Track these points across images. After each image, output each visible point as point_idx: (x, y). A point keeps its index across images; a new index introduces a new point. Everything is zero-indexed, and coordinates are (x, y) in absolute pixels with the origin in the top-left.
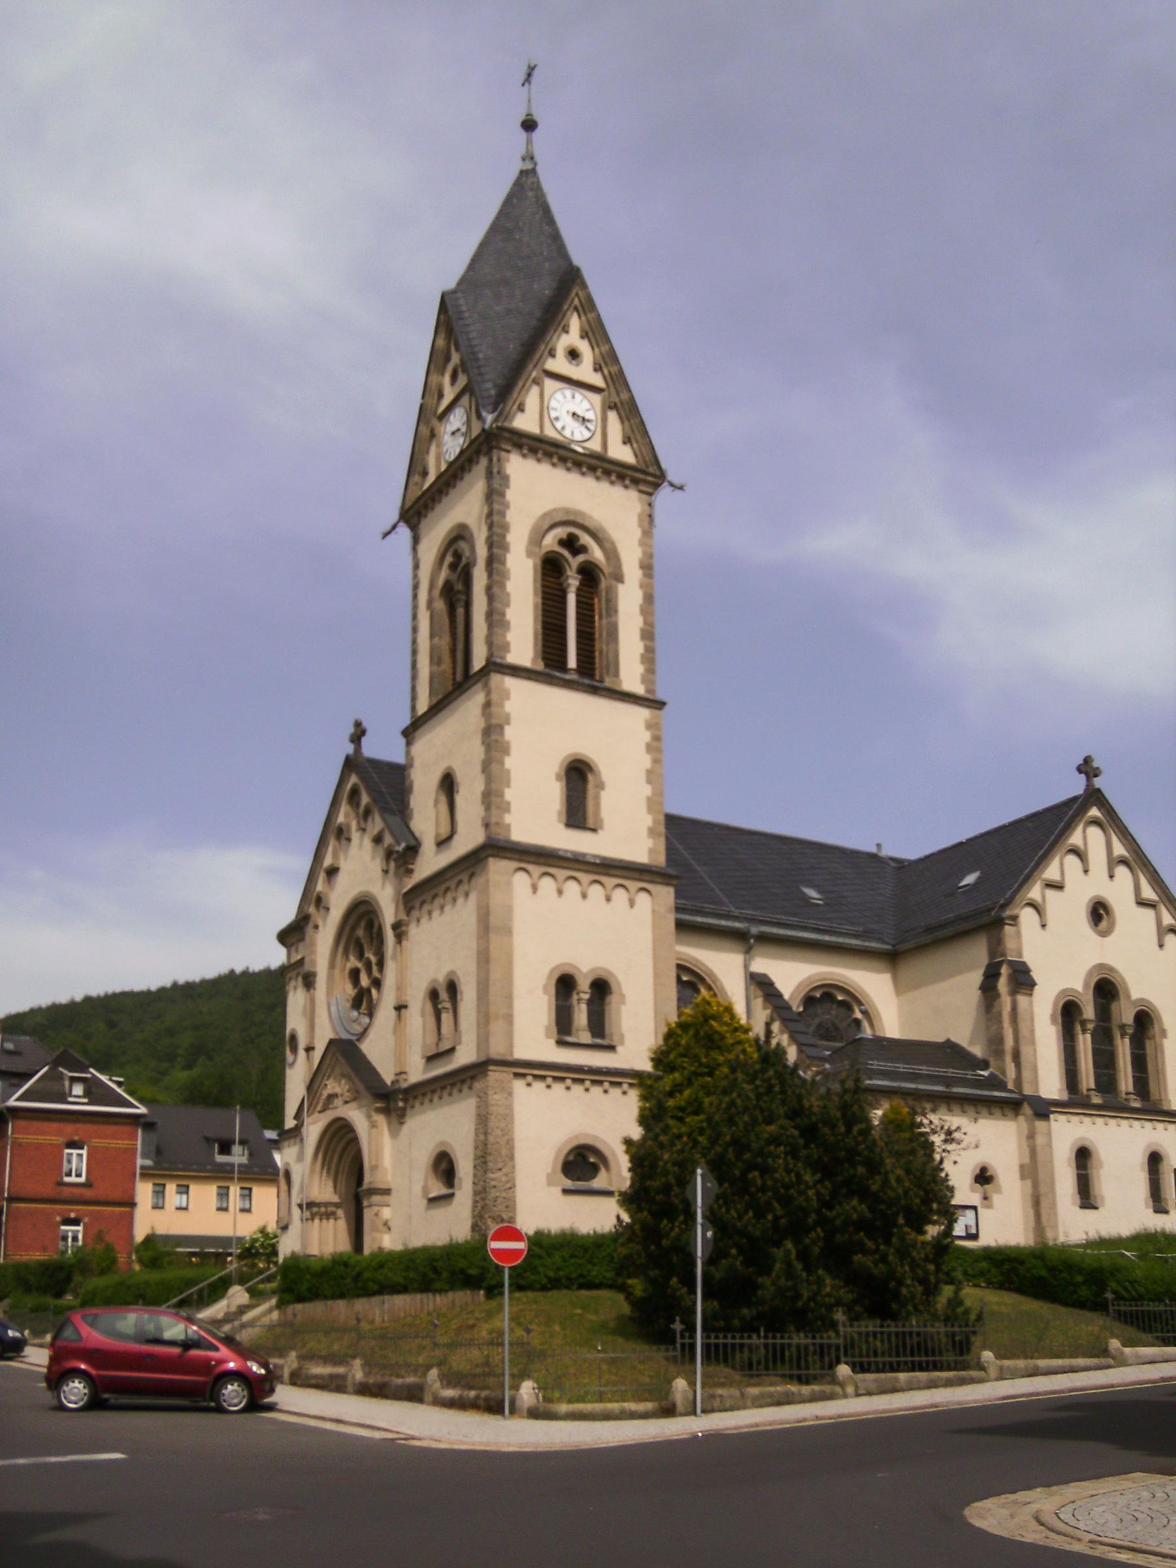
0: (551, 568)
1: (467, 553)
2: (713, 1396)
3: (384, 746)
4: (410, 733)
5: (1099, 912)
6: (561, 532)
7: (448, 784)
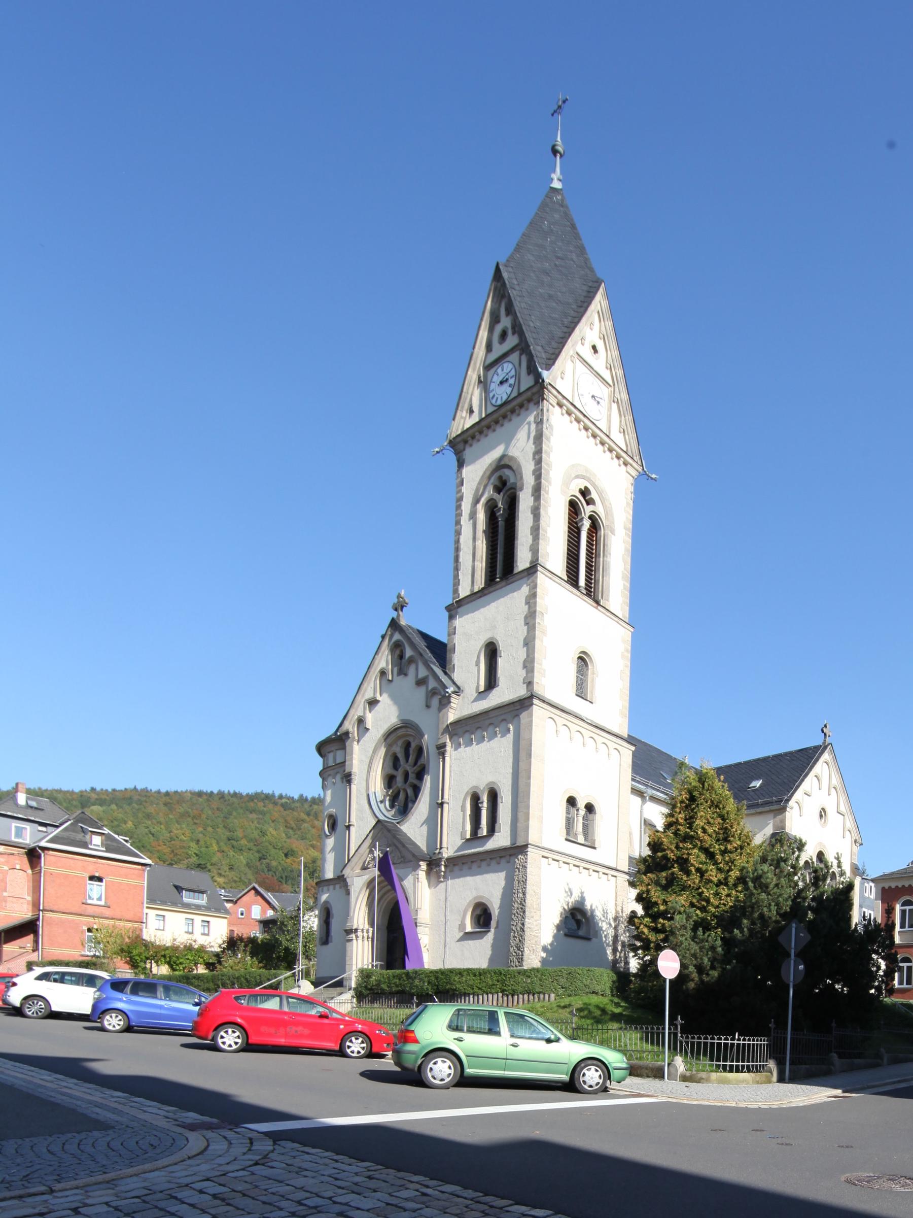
0: (573, 506)
1: (512, 480)
2: (212, 1040)
3: (426, 618)
4: (454, 609)
5: (823, 814)
6: (582, 484)
7: (492, 652)
